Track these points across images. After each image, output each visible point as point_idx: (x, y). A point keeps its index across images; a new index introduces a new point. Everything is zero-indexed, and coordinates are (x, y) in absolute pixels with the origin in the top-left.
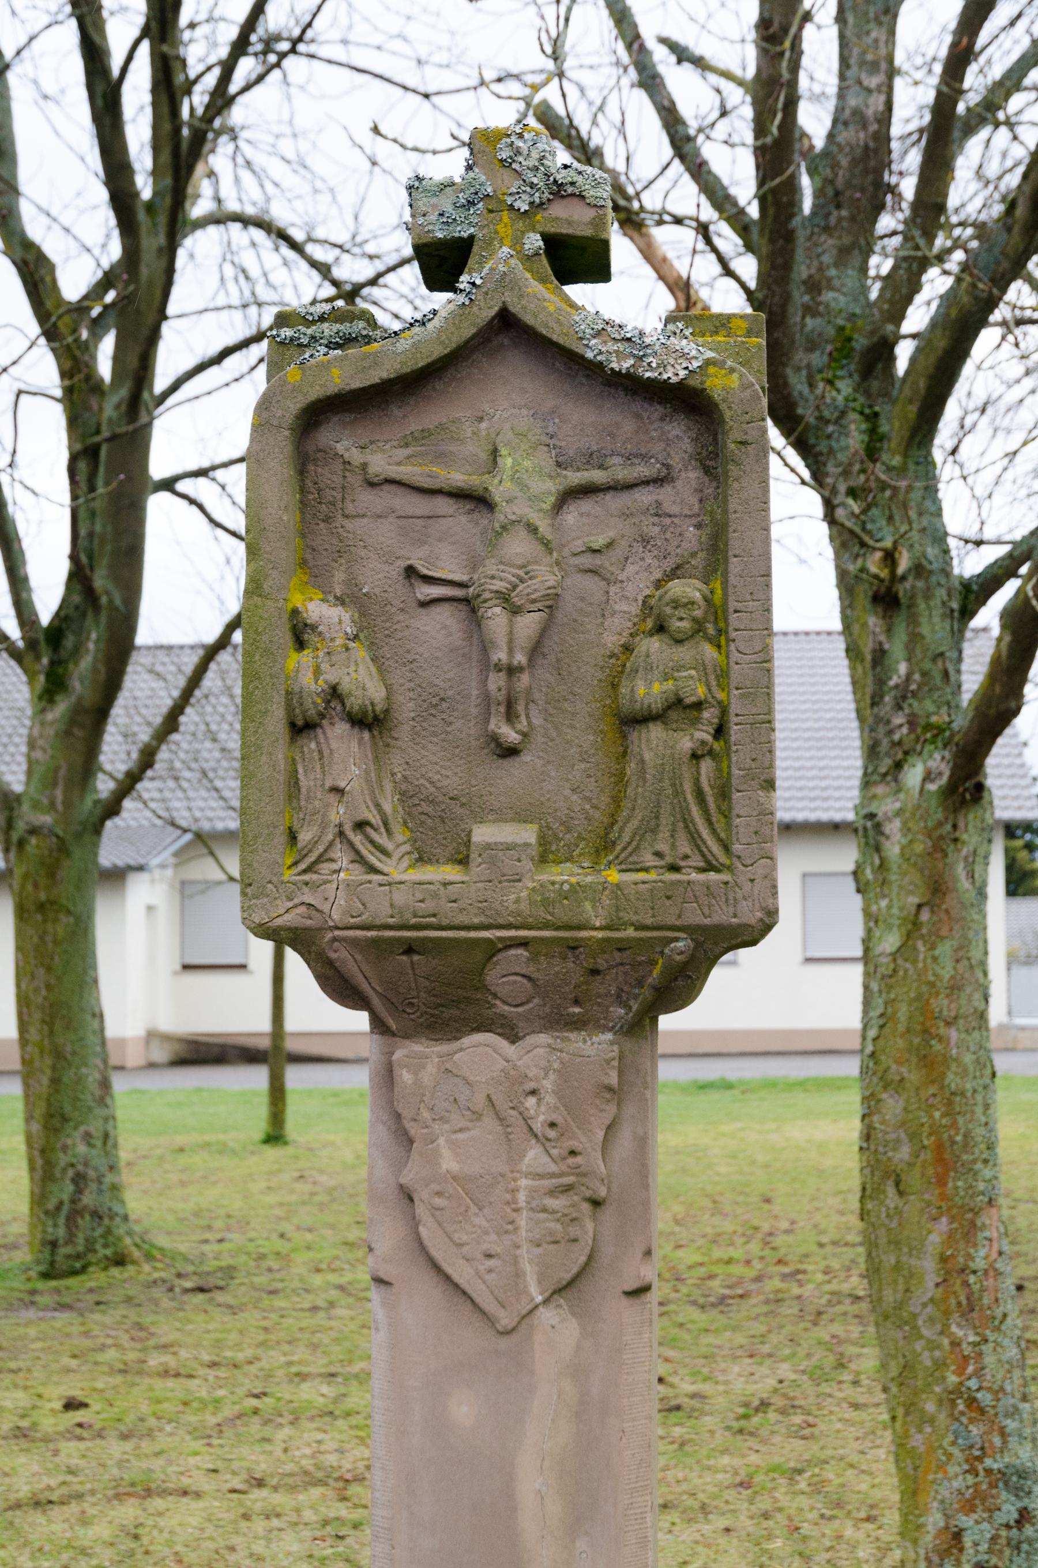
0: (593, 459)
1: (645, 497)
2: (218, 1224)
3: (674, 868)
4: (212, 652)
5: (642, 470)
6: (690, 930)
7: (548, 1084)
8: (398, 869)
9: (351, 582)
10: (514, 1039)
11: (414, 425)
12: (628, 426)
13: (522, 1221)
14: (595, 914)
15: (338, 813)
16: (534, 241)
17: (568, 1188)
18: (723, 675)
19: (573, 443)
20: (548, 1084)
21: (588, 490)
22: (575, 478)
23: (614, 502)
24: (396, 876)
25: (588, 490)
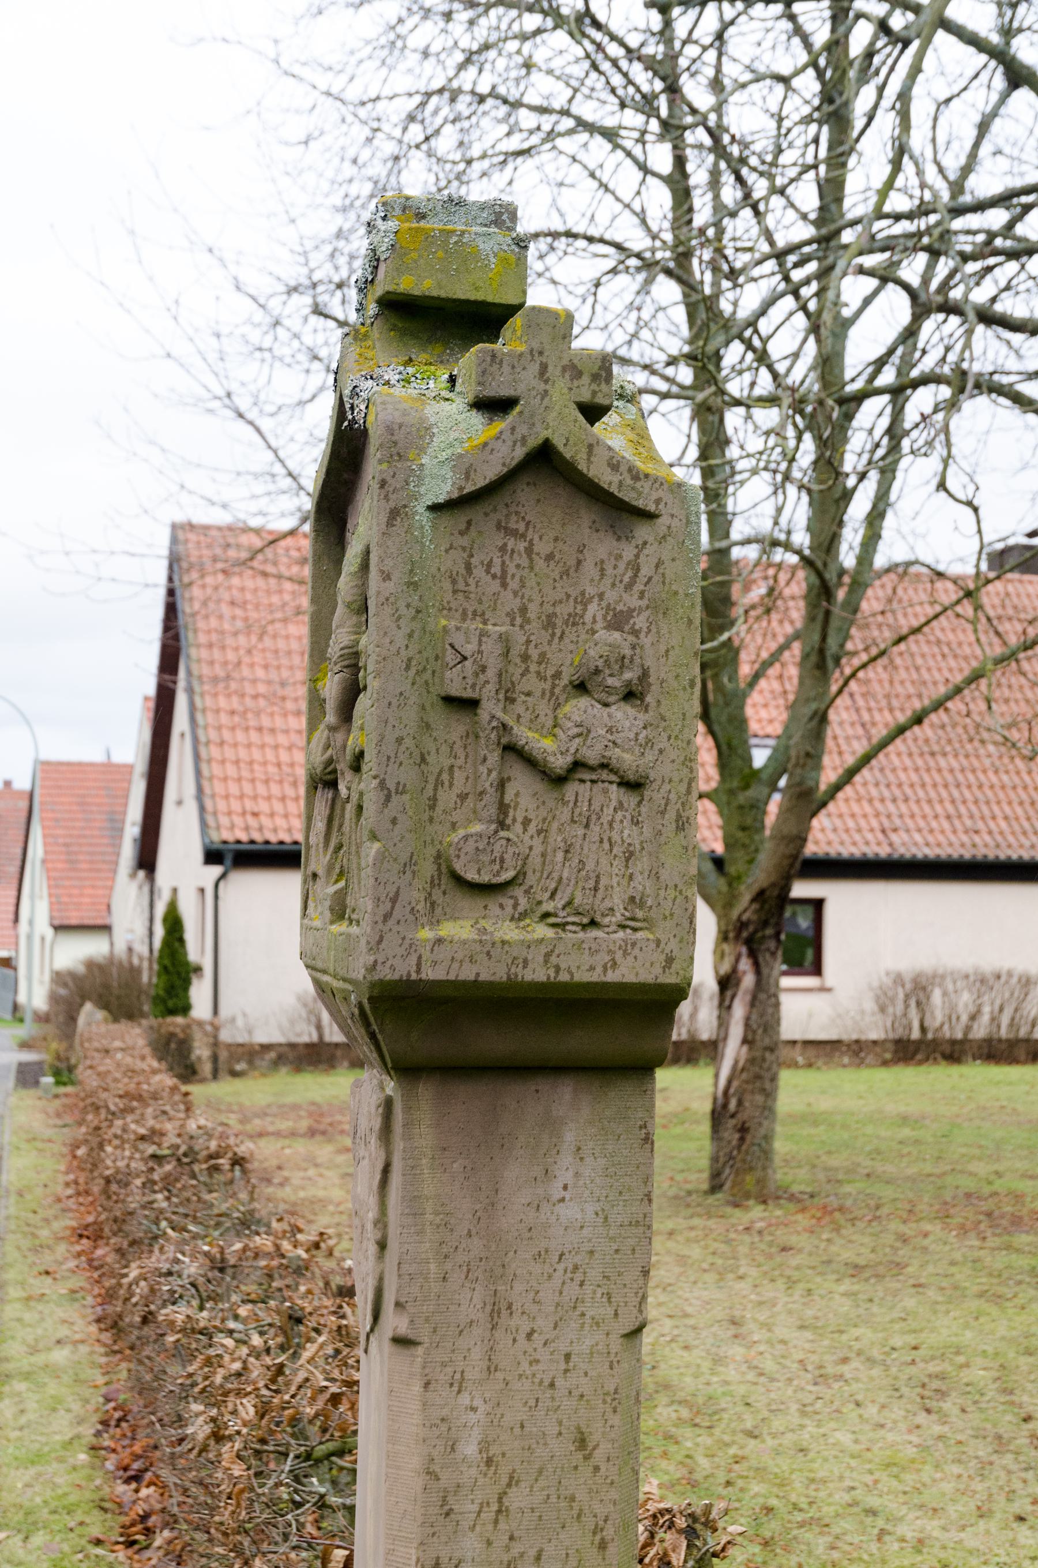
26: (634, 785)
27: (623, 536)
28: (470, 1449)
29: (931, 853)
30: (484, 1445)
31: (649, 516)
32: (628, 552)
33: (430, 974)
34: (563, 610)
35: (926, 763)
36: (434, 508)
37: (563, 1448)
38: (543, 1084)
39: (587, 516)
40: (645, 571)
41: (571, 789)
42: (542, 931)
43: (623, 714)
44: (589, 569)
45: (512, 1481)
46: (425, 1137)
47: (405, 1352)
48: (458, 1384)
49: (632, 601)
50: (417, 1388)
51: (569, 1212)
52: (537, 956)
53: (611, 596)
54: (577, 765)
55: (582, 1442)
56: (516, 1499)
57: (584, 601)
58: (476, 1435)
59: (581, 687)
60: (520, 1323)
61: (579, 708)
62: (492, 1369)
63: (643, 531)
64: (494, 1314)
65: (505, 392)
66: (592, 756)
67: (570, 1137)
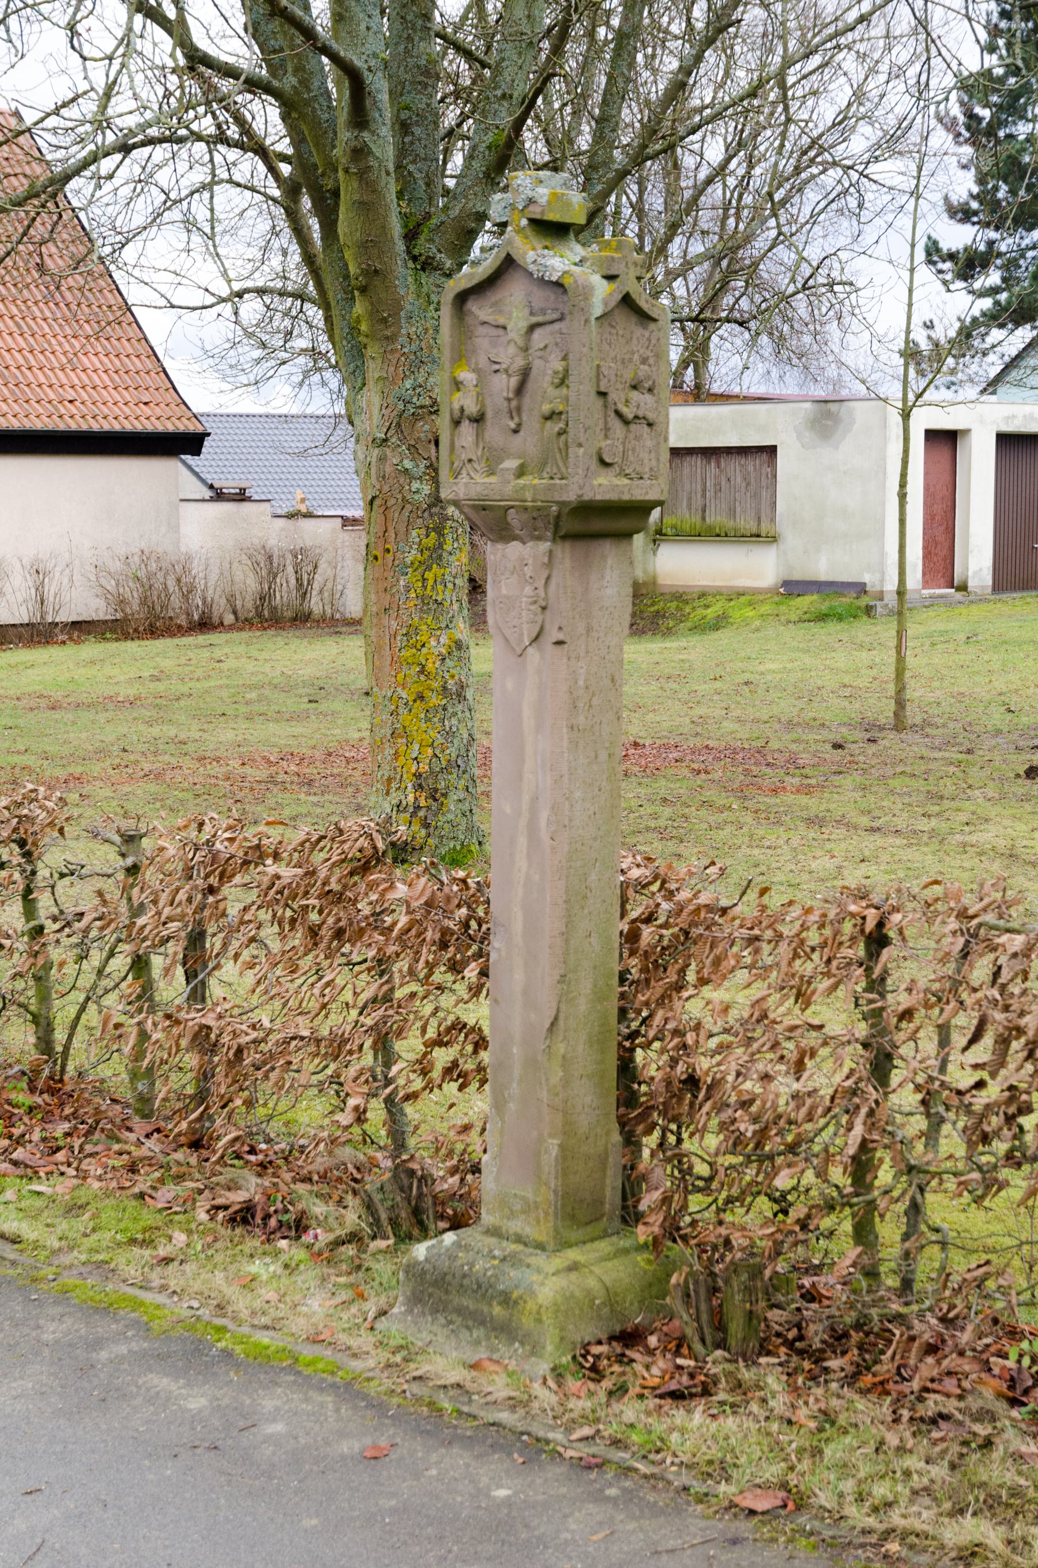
0: (543, 311)
1: (557, 326)
2: (806, 694)
3: (552, 478)
4: (914, 405)
5: (555, 316)
6: (557, 503)
7: (530, 562)
8: (479, 479)
9: (476, 364)
10: (524, 543)
11: (493, 300)
12: (553, 297)
13: (524, 613)
14: (528, 496)
15: (464, 457)
16: (524, 222)
17: (535, 602)
18: (567, 399)
19: (537, 305)
20: (530, 562)
21: (539, 325)
22: (534, 320)
23: (548, 328)
24: (479, 480)
25: (539, 325)
26: (650, 425)
27: (645, 328)
28: (581, 683)
29: (38, 425)
30: (586, 680)
31: (655, 320)
32: (647, 334)
33: (598, 497)
34: (627, 357)
35: (104, 347)
36: (597, 319)
37: (607, 682)
38: (601, 542)
39: (634, 319)
40: (653, 342)
41: (633, 427)
42: (626, 481)
43: (648, 397)
44: (635, 341)
45: (593, 695)
46: (568, 563)
47: (559, 648)
48: (578, 658)
49: (649, 353)
50: (565, 660)
51: (609, 591)
52: (626, 490)
53: (642, 351)
54: (636, 417)
55: (613, 680)
56: (595, 701)
57: (633, 353)
58: (583, 677)
59: (634, 387)
60: (594, 634)
61: (634, 395)
62: (587, 652)
63: (652, 326)
64: (588, 631)
65: (615, 273)
66: (640, 414)
67: (609, 562)
